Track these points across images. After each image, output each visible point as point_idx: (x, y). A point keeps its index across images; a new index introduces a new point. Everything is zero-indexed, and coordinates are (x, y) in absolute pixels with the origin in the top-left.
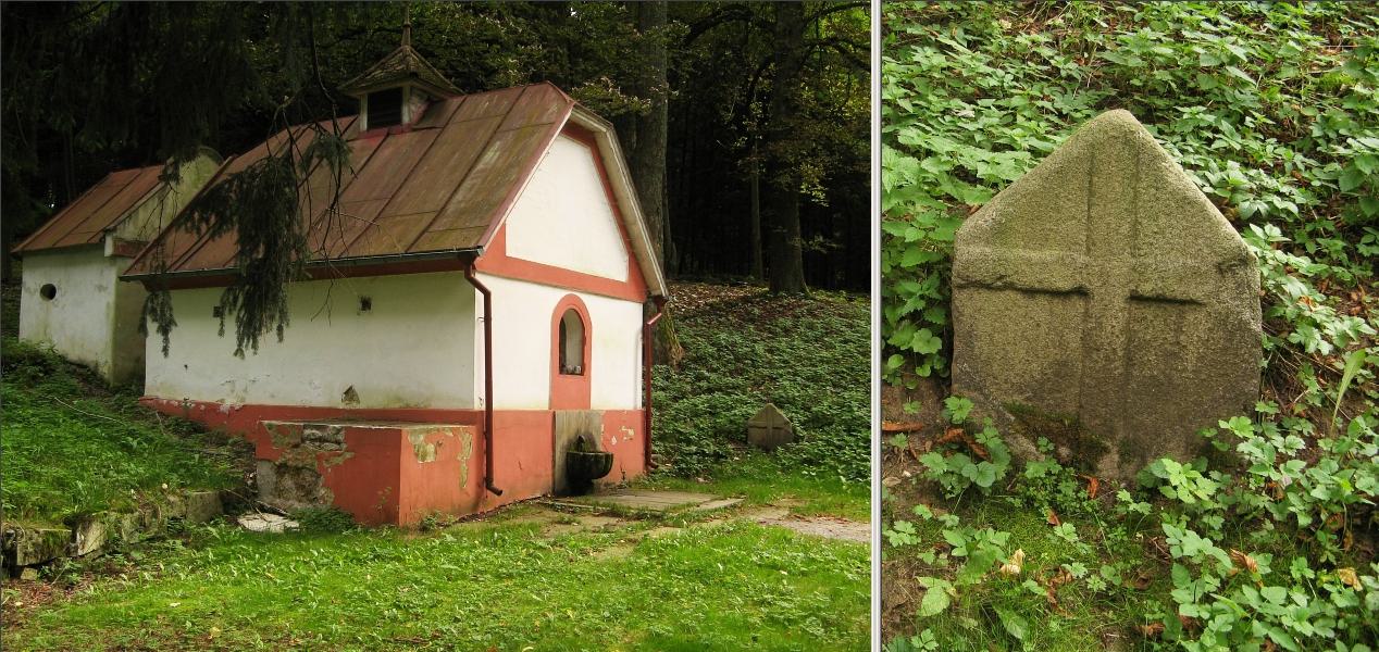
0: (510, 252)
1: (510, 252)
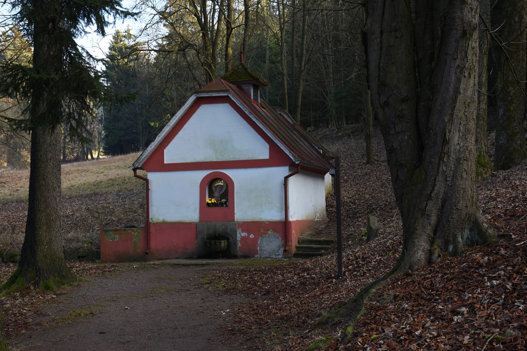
0: (165, 163)
1: (165, 163)
